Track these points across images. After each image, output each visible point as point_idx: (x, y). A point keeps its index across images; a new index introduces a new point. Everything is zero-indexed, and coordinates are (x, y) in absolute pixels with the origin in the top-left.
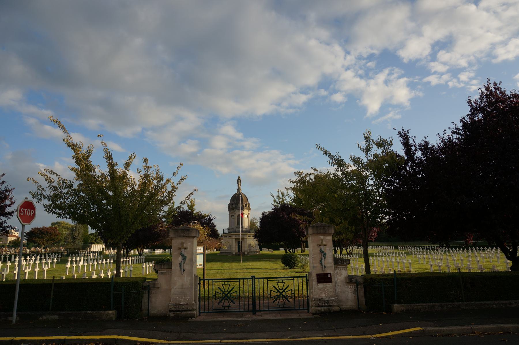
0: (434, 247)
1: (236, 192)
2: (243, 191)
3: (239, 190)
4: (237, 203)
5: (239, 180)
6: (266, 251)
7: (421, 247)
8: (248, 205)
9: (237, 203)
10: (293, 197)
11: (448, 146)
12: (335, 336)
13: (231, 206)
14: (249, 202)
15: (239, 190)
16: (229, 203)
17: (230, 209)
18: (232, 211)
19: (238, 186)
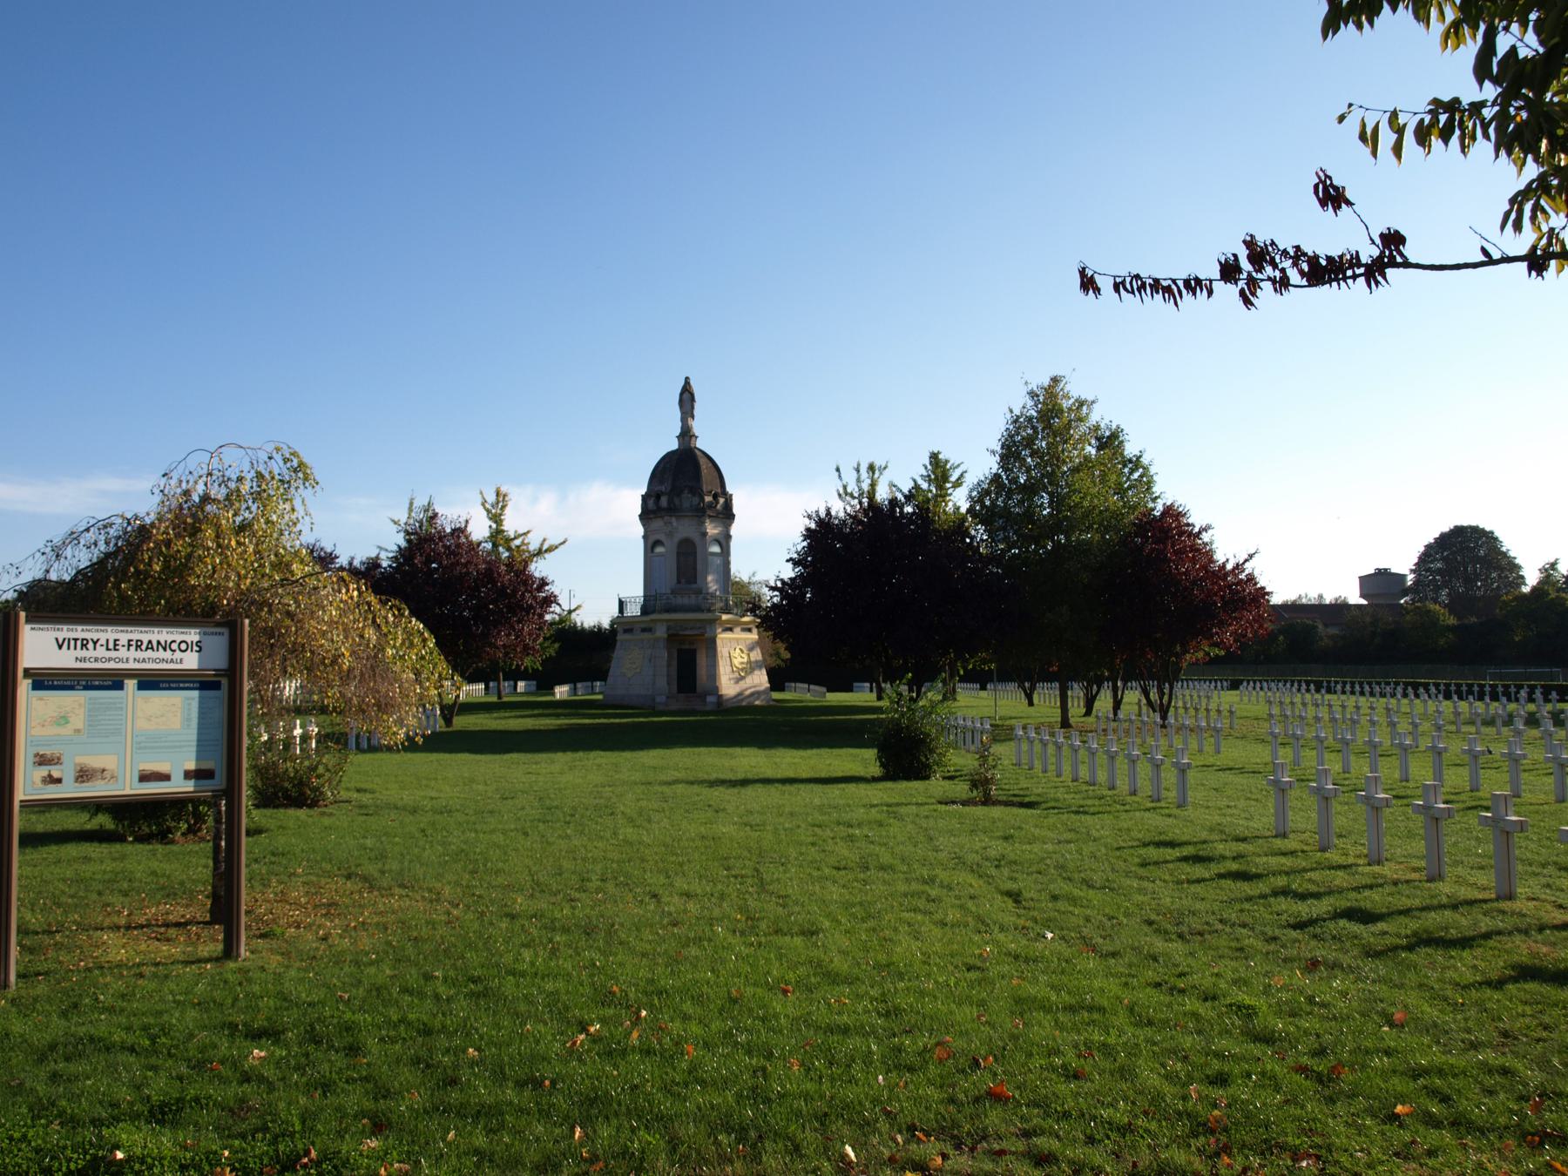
0: (1353, 684)
1: (674, 445)
2: (700, 444)
3: (686, 434)
4: (685, 493)
5: (687, 398)
6: (800, 694)
7: (1426, 687)
8: (722, 500)
9: (685, 493)
10: (882, 494)
11: (583, 629)
12: (600, 716)
13: (651, 502)
14: (729, 489)
15: (686, 434)
16: (644, 491)
17: (645, 516)
18: (657, 524)
19: (684, 420)
